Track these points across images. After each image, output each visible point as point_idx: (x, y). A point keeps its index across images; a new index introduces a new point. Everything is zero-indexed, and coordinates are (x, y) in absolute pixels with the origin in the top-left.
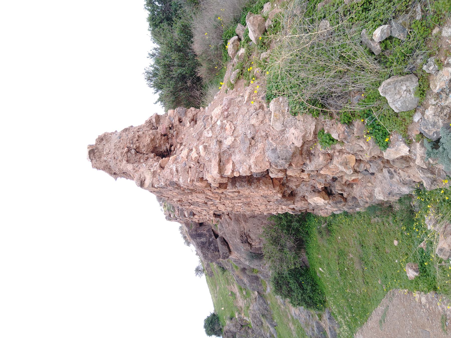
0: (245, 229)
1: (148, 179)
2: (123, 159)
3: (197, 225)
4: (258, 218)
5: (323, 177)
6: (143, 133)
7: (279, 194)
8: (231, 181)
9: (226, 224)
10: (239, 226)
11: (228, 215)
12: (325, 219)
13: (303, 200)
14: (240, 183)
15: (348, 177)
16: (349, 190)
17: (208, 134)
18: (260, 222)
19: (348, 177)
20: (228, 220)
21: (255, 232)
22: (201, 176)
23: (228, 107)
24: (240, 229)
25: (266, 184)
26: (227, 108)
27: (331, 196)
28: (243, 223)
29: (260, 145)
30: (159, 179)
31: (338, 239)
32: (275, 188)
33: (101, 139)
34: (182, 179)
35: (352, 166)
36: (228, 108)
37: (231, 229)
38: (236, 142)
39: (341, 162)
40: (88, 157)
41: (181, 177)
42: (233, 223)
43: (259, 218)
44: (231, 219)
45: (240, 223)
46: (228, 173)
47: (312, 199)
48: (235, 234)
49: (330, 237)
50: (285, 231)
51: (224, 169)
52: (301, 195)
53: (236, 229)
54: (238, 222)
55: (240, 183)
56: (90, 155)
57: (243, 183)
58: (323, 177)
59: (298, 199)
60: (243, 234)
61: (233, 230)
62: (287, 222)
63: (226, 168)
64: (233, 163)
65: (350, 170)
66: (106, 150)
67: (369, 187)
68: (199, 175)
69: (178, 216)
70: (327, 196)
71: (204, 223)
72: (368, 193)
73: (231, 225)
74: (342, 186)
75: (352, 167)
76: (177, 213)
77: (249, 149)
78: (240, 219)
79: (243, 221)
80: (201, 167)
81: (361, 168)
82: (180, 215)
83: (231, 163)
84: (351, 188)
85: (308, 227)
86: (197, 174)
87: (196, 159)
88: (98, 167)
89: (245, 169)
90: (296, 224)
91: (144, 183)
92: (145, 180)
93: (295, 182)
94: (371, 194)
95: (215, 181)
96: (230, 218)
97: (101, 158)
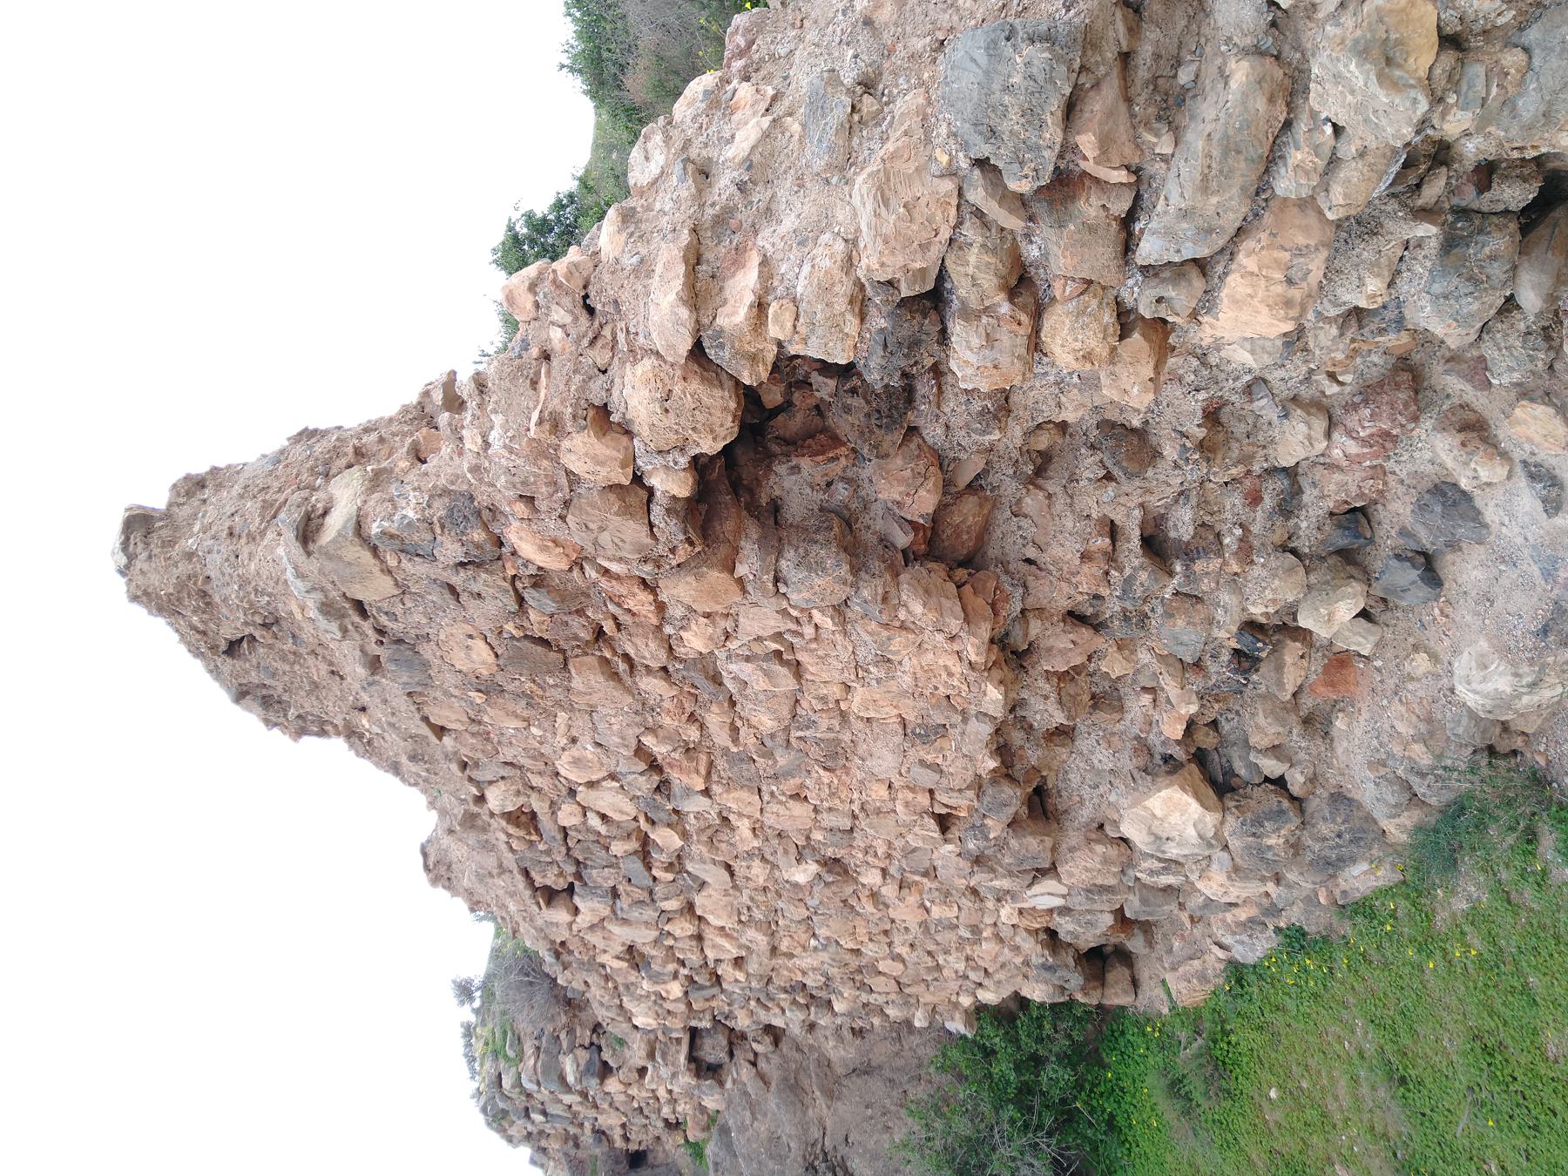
0: (828, 1132)
1: (343, 504)
2: (266, 528)
3: (617, 1162)
4: (887, 1073)
5: (1197, 620)
6: (381, 440)
7: (990, 687)
8: (755, 536)
9: (744, 1109)
10: (799, 1114)
11: (754, 1064)
12: (1192, 1018)
13: (1098, 841)
14: (801, 551)
15: (1316, 609)
16: (1314, 752)
17: (647, 158)
18: (895, 1093)
19: (1316, 609)
20: (753, 1087)
21: (871, 1145)
22: (596, 395)
23: (750, 37)
24: (806, 1131)
25: (927, 592)
26: (743, 44)
27: (1229, 795)
28: (821, 1101)
29: (907, 103)
30: (398, 496)
31: (1265, 1104)
32: (972, 626)
33: (194, 486)
34: (502, 426)
35: (1423, 73)
36: (751, 43)
37: (764, 1135)
38: (783, 133)
39: (1356, 41)
40: (118, 545)
41: (498, 419)
42: (772, 1102)
43: (890, 1075)
44: (767, 1083)
45: (807, 1100)
46: (734, 313)
47: (1139, 810)
48: (781, 1159)
49: (1228, 1104)
50: (1010, 1111)
51: (718, 299)
52: (1085, 814)
53: (788, 1130)
54: (796, 1095)
55: (801, 551)
56: (127, 539)
57: (816, 547)
58: (1197, 620)
59: (1073, 842)
60: (816, 1158)
61: (774, 1140)
62: (1018, 1068)
63: (727, 293)
64: (765, 262)
65: (1413, 93)
66: (203, 516)
67: (1419, 680)
68: (591, 384)
69: (534, 1078)
70: (1211, 792)
71: (650, 1157)
72: (1414, 718)
73: (765, 1115)
74: (1283, 714)
75: (1419, 79)
76: (532, 1062)
77: (850, 139)
78: (805, 1082)
79: (818, 1093)
80: (600, 343)
81: (1471, 94)
82: (543, 1073)
83: (754, 259)
84: (1319, 741)
85: (1116, 1091)
86: (578, 378)
87: (574, 270)
88: (150, 590)
89: (823, 264)
90: (1060, 1073)
91: (320, 527)
92: (325, 513)
93: (1063, 652)
94: (1429, 720)
95: (667, 405)
96: (762, 1077)
97: (173, 547)
